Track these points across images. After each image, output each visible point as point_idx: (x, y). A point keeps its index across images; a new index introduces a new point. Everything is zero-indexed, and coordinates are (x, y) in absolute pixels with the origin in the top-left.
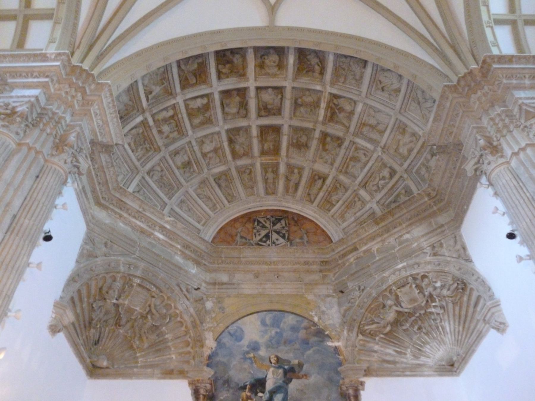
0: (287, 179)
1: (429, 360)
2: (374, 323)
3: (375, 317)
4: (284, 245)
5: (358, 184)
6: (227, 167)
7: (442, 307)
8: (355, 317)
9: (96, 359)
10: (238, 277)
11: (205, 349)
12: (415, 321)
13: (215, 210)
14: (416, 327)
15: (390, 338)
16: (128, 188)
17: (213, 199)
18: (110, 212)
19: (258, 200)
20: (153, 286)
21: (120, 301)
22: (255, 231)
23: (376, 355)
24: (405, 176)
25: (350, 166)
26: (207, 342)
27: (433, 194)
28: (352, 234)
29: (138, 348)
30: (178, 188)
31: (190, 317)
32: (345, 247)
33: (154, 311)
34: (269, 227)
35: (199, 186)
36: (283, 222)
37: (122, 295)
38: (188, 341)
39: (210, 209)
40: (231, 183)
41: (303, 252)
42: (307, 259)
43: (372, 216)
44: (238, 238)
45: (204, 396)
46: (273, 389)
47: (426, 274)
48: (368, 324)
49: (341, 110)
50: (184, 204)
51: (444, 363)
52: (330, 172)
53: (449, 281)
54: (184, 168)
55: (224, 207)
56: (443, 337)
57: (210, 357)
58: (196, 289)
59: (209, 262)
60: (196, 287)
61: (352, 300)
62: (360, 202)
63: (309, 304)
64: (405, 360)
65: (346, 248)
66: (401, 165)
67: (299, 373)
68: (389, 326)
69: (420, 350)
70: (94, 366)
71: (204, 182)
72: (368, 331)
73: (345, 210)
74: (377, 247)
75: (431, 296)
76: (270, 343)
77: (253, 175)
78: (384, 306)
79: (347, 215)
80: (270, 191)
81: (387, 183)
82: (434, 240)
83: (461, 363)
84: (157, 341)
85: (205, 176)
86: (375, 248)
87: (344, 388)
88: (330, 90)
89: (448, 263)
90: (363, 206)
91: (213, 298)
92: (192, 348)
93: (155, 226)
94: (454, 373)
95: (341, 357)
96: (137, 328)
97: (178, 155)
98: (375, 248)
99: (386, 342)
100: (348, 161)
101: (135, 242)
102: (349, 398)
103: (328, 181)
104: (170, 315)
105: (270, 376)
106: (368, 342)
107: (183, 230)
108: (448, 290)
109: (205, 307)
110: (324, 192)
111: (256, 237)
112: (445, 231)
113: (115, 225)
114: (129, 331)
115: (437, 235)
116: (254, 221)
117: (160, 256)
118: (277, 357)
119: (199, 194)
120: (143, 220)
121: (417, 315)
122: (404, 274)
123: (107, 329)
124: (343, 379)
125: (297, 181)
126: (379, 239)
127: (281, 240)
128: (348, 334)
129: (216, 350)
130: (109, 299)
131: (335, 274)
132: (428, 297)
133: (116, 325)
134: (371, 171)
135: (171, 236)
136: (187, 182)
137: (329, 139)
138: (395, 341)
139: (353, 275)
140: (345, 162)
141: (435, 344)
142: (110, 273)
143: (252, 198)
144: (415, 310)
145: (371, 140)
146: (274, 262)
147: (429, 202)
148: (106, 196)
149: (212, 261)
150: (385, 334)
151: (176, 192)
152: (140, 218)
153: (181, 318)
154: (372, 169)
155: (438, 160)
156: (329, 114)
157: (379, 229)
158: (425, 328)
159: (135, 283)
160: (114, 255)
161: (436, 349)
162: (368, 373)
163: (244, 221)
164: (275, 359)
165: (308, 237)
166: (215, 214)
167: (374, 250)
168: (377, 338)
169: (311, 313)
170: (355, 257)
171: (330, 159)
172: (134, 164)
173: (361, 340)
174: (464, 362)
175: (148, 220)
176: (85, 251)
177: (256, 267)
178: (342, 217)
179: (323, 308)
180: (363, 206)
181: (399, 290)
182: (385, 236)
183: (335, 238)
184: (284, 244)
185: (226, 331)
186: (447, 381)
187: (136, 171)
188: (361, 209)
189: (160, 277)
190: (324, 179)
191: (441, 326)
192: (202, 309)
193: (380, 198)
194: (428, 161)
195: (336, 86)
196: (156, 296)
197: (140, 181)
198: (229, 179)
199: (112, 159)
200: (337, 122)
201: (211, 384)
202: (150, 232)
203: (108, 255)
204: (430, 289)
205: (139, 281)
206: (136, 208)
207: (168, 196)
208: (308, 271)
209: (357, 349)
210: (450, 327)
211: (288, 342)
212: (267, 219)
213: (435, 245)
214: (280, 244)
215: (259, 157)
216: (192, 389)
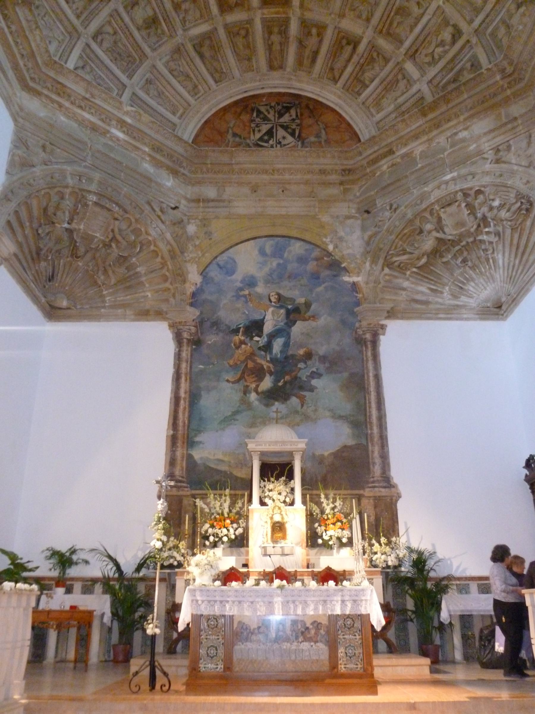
0: (301, 44)
1: (471, 301)
2: (404, 252)
3: (407, 245)
4: (294, 146)
5: (404, 53)
6: (212, 26)
7: (497, 234)
8: (381, 246)
9: (53, 299)
10: (230, 191)
11: (187, 285)
12: (460, 251)
13: (196, 94)
14: (460, 260)
15: (425, 272)
16: (66, 63)
17: (194, 78)
18: (44, 101)
19: (258, 78)
20: (114, 205)
21: (74, 226)
22: (253, 125)
23: (404, 293)
24: (474, 40)
25: (395, 24)
26: (190, 276)
27: (509, 70)
28: (387, 130)
29: (103, 284)
30: (141, 60)
31: (167, 245)
32: (376, 148)
33: (119, 237)
34: (272, 119)
35: (172, 57)
36: (293, 112)
37: (75, 217)
38: (166, 276)
39: (189, 92)
40: (219, 51)
41: (318, 157)
42: (323, 166)
43: (420, 102)
44: (230, 137)
46: (272, 332)
47: (482, 189)
50: (151, 86)
51: (489, 305)
52: (364, 33)
53: (512, 199)
54: (147, 28)
55: (210, 89)
56: (492, 272)
57: (194, 295)
59: (191, 172)
60: (173, 206)
61: (380, 223)
62: (405, 81)
63: (322, 227)
64: (440, 300)
65: (378, 150)
66: (471, 21)
67: (305, 314)
68: (425, 257)
69: (461, 288)
70: (52, 307)
71: (178, 50)
72: (396, 264)
73: (383, 93)
74: (421, 149)
75: (484, 218)
76: (270, 278)
77: (250, 37)
78: (421, 232)
79: (384, 102)
81: (446, 52)
82: (499, 140)
83: (510, 306)
84: (127, 275)
85: (180, 41)
86: (417, 152)
87: (360, 332)
89: (513, 173)
90: (408, 86)
91: (197, 220)
92: (171, 284)
93: (110, 120)
94: (501, 317)
95: (360, 296)
96: (100, 260)
97: (136, 8)
98: (417, 152)
99: (419, 277)
100: (392, 14)
101: (85, 144)
103: (362, 47)
104: (140, 243)
105: (269, 317)
106: (396, 277)
107: (151, 125)
108: (508, 211)
109: (186, 232)
110: (354, 66)
111: (254, 134)
112: (517, 126)
113: (54, 119)
114: (90, 264)
115: (504, 133)
116: (253, 110)
117: (121, 163)
118: (278, 294)
119: (172, 70)
120: (93, 111)
121: (464, 243)
122: (452, 188)
123: (62, 261)
124: (360, 321)
125: (314, 48)
126: (425, 138)
127: (290, 139)
128: (371, 266)
129: (202, 286)
130: (59, 224)
131: (361, 187)
132: (480, 220)
134: (426, 32)
135: (135, 134)
136: (154, 50)
138: (429, 276)
140: (388, 16)
141: (482, 281)
142: (55, 187)
143: (250, 75)
144: (461, 236)
146: (278, 170)
147: (501, 83)
148: (36, 76)
149: (193, 169)
150: (418, 268)
151: (138, 67)
152: (87, 109)
153: (155, 246)
154: (427, 28)
155: (524, 15)
157: (426, 122)
158: (472, 261)
159: (90, 201)
160: (57, 163)
161: (483, 288)
162: (392, 314)
163: (239, 110)
164: (276, 297)
165: (326, 133)
166: (196, 100)
167: (416, 154)
168: (408, 273)
169: (324, 240)
170: (390, 164)
171: (366, 13)
172: (71, 23)
173: (386, 275)
174: (514, 303)
175: (98, 111)
176: (17, 158)
177: (253, 178)
178: (378, 104)
179: (342, 234)
180: (408, 86)
181: (442, 210)
182: (435, 132)
183: (365, 136)
184: (293, 144)
185: (214, 262)
187: (75, 35)
188: (405, 93)
189: (123, 192)
190: (354, 43)
191: (492, 258)
192: (182, 234)
193: (433, 75)
194: (511, 17)
196: (120, 218)
197: (84, 50)
198: (216, 45)
199: (34, 16)
201: (196, 327)
202: (104, 129)
203: (49, 163)
204: (485, 209)
205: (95, 198)
206: (79, 92)
207: (127, 74)
208: (324, 184)
209: (380, 286)
210: (503, 260)
212: (271, 107)
213: (500, 148)
214: (288, 144)
216: (173, 332)
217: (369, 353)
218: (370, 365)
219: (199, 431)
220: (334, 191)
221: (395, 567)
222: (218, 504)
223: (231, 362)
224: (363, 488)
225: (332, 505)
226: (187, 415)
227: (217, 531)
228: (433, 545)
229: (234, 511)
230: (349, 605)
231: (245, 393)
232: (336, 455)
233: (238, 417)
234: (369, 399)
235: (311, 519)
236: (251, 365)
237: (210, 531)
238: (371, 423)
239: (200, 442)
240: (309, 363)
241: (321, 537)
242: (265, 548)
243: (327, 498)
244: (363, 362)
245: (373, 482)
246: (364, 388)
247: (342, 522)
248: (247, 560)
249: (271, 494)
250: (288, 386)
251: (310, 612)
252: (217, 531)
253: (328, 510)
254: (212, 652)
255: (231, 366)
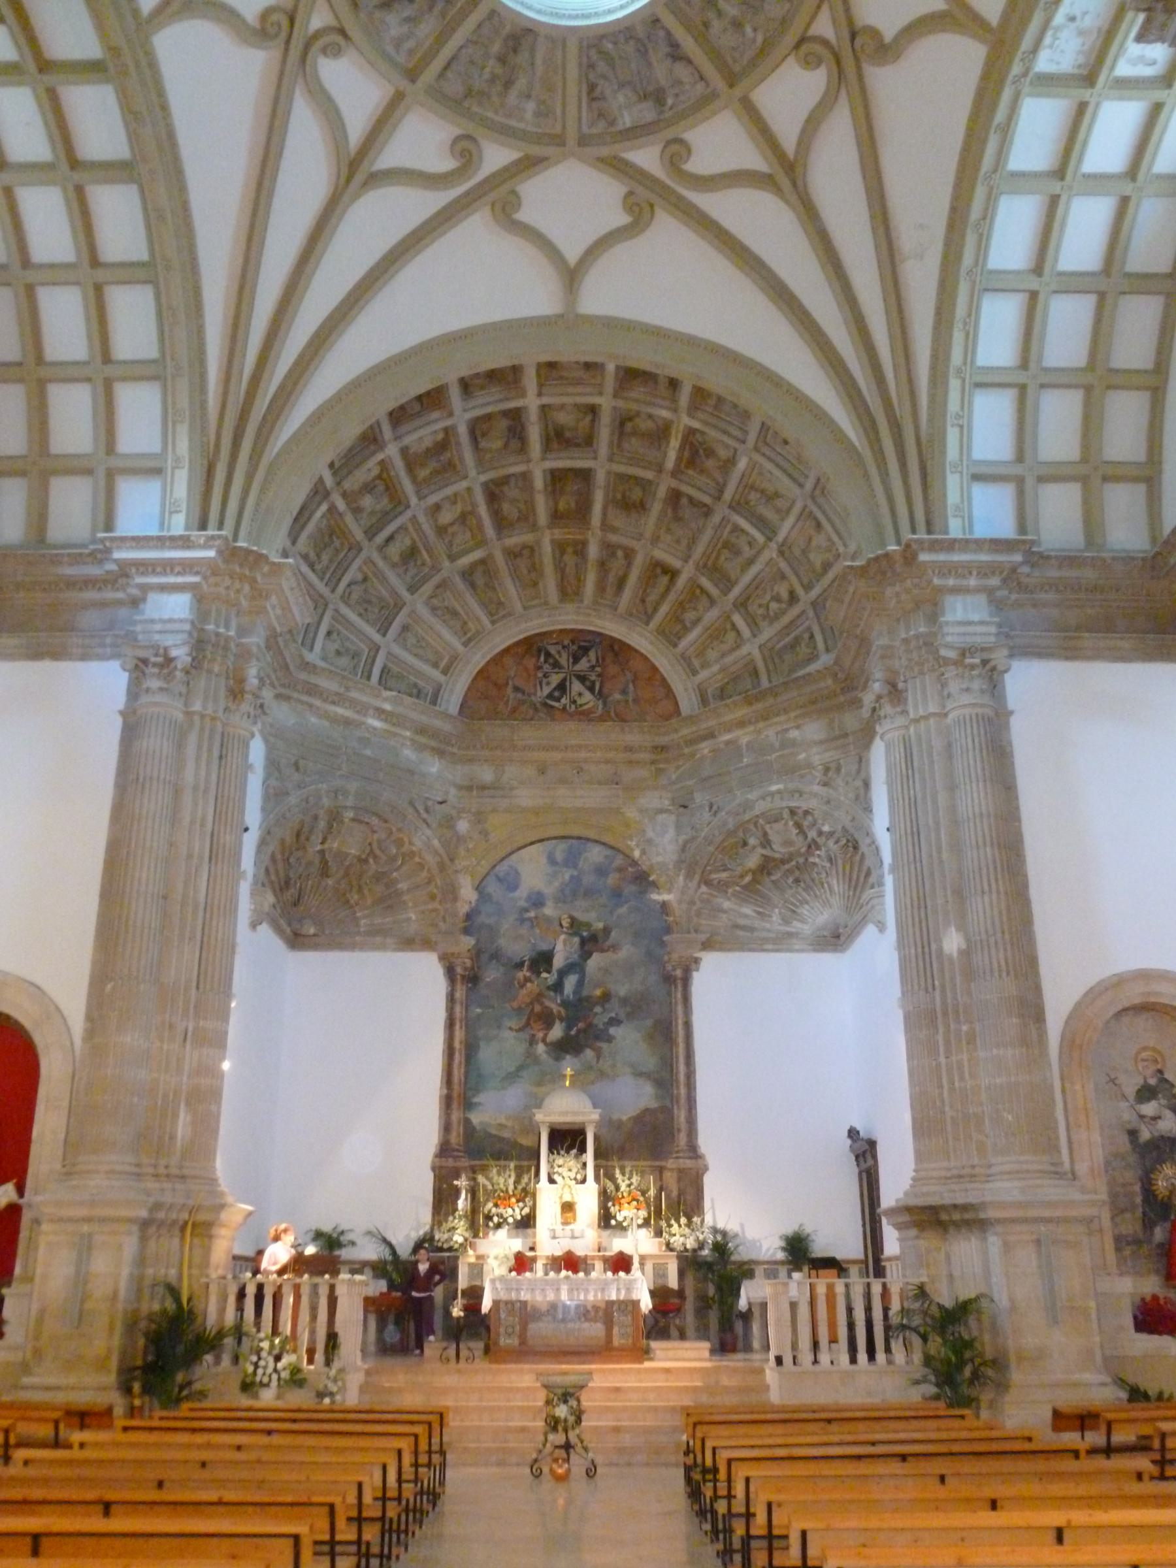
1: (806, 927)
10: (511, 772)
11: (459, 904)
14: (790, 880)
25: (722, 558)
33: (378, 852)
36: (592, 654)
45: (463, 977)
48: (717, 871)
49: (710, 453)
57: (468, 917)
58: (441, 803)
60: (440, 799)
64: (768, 926)
69: (794, 912)
70: (296, 934)
78: (745, 844)
79: (712, 655)
80: (569, 591)
87: (669, 968)
88: (686, 421)
92: (440, 902)
98: (744, 740)
102: (675, 981)
103: (681, 581)
105: (559, 947)
116: (539, 651)
120: (347, 704)
122: (779, 803)
124: (669, 953)
126: (751, 728)
129: (477, 905)
131: (678, 768)
133: (322, 875)
137: (684, 501)
139: (704, 780)
145: (761, 523)
156: (687, 454)
162: (707, 946)
177: (542, 755)
179: (650, 834)
184: (591, 704)
186: (828, 959)
190: (673, 574)
195: (700, 415)
197: (333, 618)
200: (702, 471)
209: (695, 908)
211: (588, 893)
212: (564, 647)
215: (549, 528)
217: (679, 995)
218: (680, 1009)
219: (477, 1091)
220: (644, 773)
221: (694, 1250)
222: (502, 1180)
223: (515, 1005)
224: (666, 1159)
225: (627, 1182)
226: (463, 1070)
227: (501, 1210)
228: (742, 1226)
229: (520, 1187)
230: (623, 1292)
231: (531, 1044)
232: (639, 1119)
233: (524, 1073)
234: (677, 1052)
235: (605, 1198)
236: (537, 1008)
237: (494, 1210)
238: (677, 1081)
239: (480, 1104)
240: (607, 1006)
241: (615, 1217)
242: (554, 1230)
243: (623, 1174)
244: (671, 1007)
245: (677, 1152)
246: (671, 1038)
247: (638, 1201)
248: (534, 1243)
249: (560, 1170)
250: (581, 1035)
251: (591, 1297)
252: (501, 1210)
253: (623, 1187)
254: (510, 1330)
255: (514, 1009)
